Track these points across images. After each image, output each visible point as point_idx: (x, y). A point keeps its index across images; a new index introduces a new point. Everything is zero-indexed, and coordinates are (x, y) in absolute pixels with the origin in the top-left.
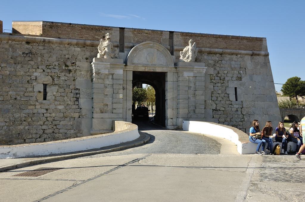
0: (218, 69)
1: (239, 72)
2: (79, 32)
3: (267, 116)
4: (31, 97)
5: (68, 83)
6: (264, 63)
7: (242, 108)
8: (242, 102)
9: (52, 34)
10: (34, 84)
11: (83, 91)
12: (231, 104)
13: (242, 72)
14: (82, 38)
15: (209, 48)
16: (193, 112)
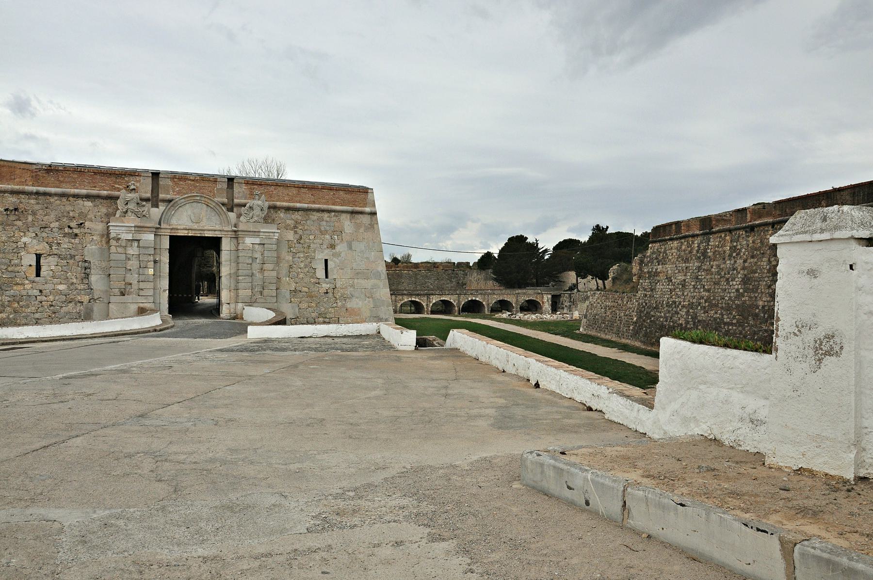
5: (73, 252)
8: (335, 279)
15: (287, 201)
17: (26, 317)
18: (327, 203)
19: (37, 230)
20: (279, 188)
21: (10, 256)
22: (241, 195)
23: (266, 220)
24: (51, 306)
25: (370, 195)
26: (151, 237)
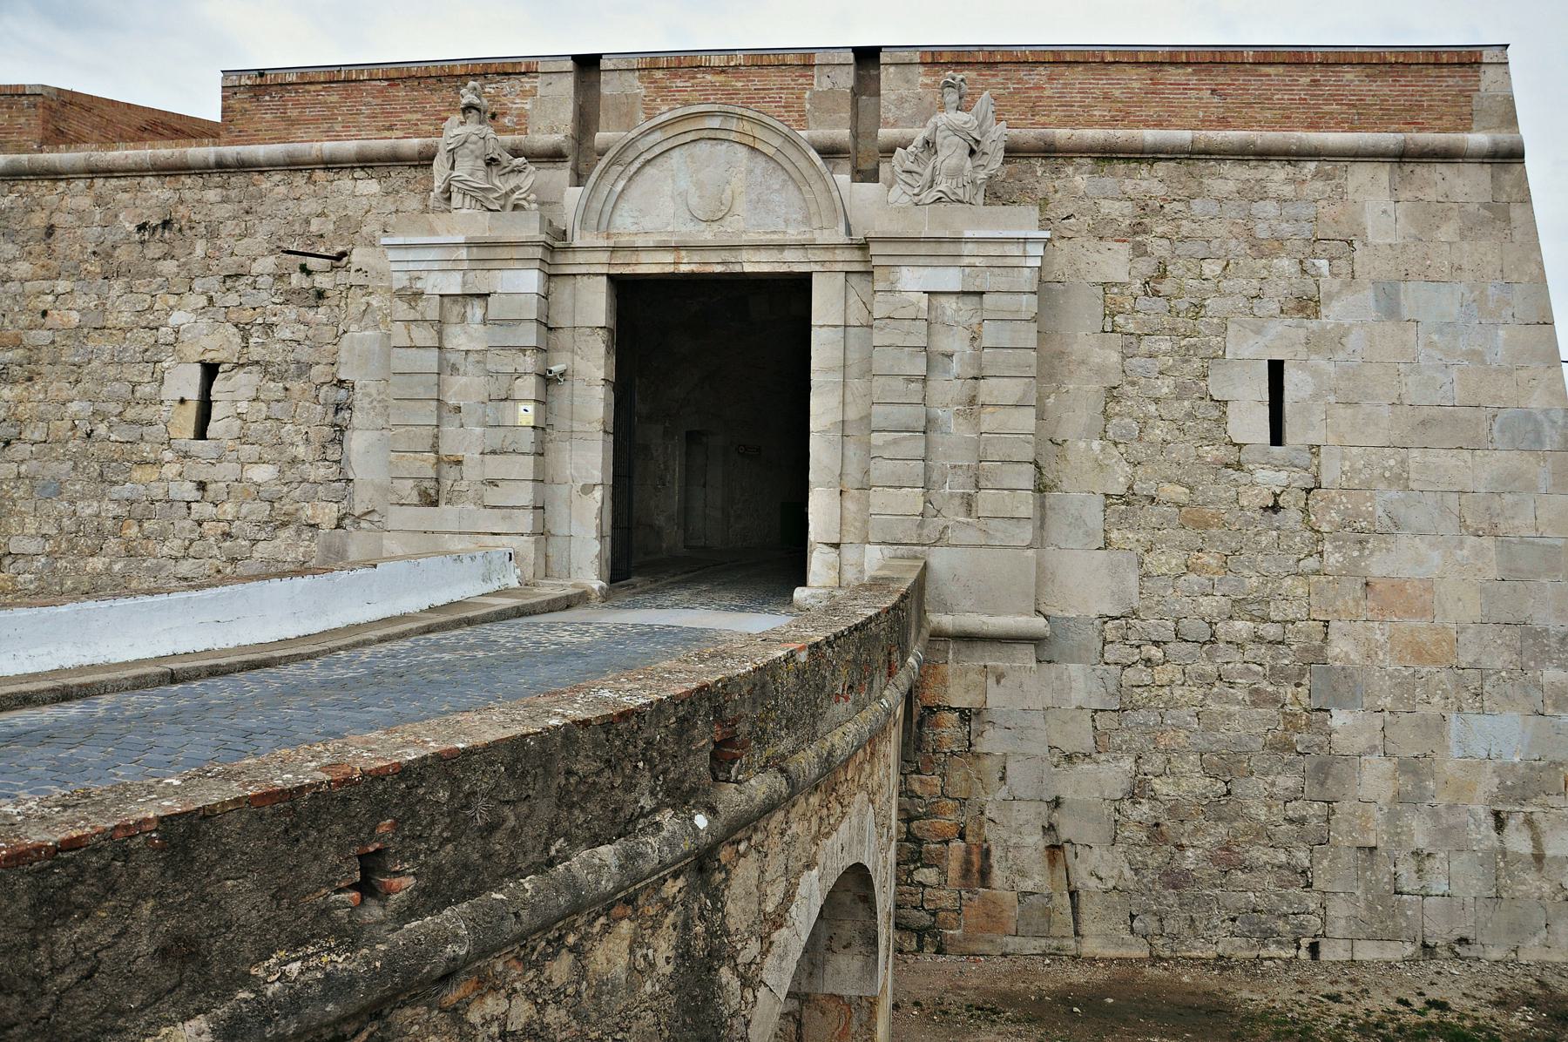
0: (1160, 248)
1: (1307, 264)
2: (379, 101)
3: (1487, 542)
4: (150, 424)
5: (304, 353)
6: (1486, 206)
7: (1308, 491)
8: (1315, 449)
9: (259, 127)
10: (165, 365)
11: (369, 395)
12: (1239, 467)
13: (1325, 262)
14: (390, 128)
15: (1103, 124)
16: (963, 509)
17: (155, 571)
18: (1285, 122)
19: (213, 283)
20: (1069, 74)
21: (132, 373)
22: (908, 110)
23: (995, 194)
24: (227, 535)
25: (1488, 76)
26: (529, 281)
